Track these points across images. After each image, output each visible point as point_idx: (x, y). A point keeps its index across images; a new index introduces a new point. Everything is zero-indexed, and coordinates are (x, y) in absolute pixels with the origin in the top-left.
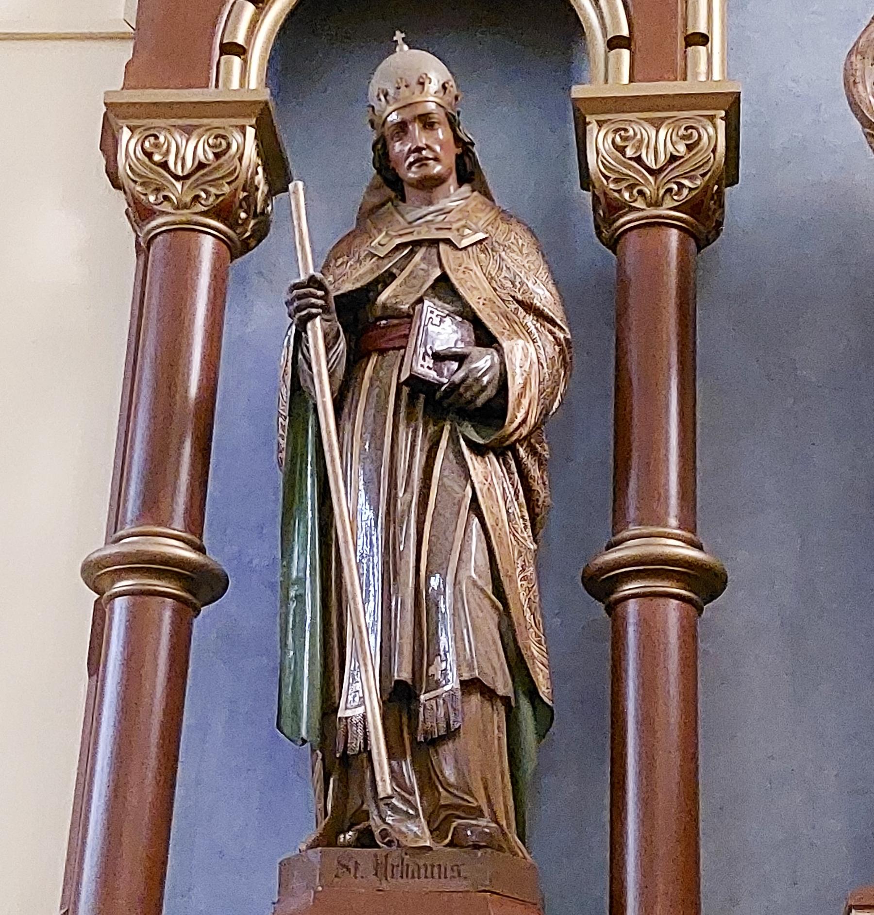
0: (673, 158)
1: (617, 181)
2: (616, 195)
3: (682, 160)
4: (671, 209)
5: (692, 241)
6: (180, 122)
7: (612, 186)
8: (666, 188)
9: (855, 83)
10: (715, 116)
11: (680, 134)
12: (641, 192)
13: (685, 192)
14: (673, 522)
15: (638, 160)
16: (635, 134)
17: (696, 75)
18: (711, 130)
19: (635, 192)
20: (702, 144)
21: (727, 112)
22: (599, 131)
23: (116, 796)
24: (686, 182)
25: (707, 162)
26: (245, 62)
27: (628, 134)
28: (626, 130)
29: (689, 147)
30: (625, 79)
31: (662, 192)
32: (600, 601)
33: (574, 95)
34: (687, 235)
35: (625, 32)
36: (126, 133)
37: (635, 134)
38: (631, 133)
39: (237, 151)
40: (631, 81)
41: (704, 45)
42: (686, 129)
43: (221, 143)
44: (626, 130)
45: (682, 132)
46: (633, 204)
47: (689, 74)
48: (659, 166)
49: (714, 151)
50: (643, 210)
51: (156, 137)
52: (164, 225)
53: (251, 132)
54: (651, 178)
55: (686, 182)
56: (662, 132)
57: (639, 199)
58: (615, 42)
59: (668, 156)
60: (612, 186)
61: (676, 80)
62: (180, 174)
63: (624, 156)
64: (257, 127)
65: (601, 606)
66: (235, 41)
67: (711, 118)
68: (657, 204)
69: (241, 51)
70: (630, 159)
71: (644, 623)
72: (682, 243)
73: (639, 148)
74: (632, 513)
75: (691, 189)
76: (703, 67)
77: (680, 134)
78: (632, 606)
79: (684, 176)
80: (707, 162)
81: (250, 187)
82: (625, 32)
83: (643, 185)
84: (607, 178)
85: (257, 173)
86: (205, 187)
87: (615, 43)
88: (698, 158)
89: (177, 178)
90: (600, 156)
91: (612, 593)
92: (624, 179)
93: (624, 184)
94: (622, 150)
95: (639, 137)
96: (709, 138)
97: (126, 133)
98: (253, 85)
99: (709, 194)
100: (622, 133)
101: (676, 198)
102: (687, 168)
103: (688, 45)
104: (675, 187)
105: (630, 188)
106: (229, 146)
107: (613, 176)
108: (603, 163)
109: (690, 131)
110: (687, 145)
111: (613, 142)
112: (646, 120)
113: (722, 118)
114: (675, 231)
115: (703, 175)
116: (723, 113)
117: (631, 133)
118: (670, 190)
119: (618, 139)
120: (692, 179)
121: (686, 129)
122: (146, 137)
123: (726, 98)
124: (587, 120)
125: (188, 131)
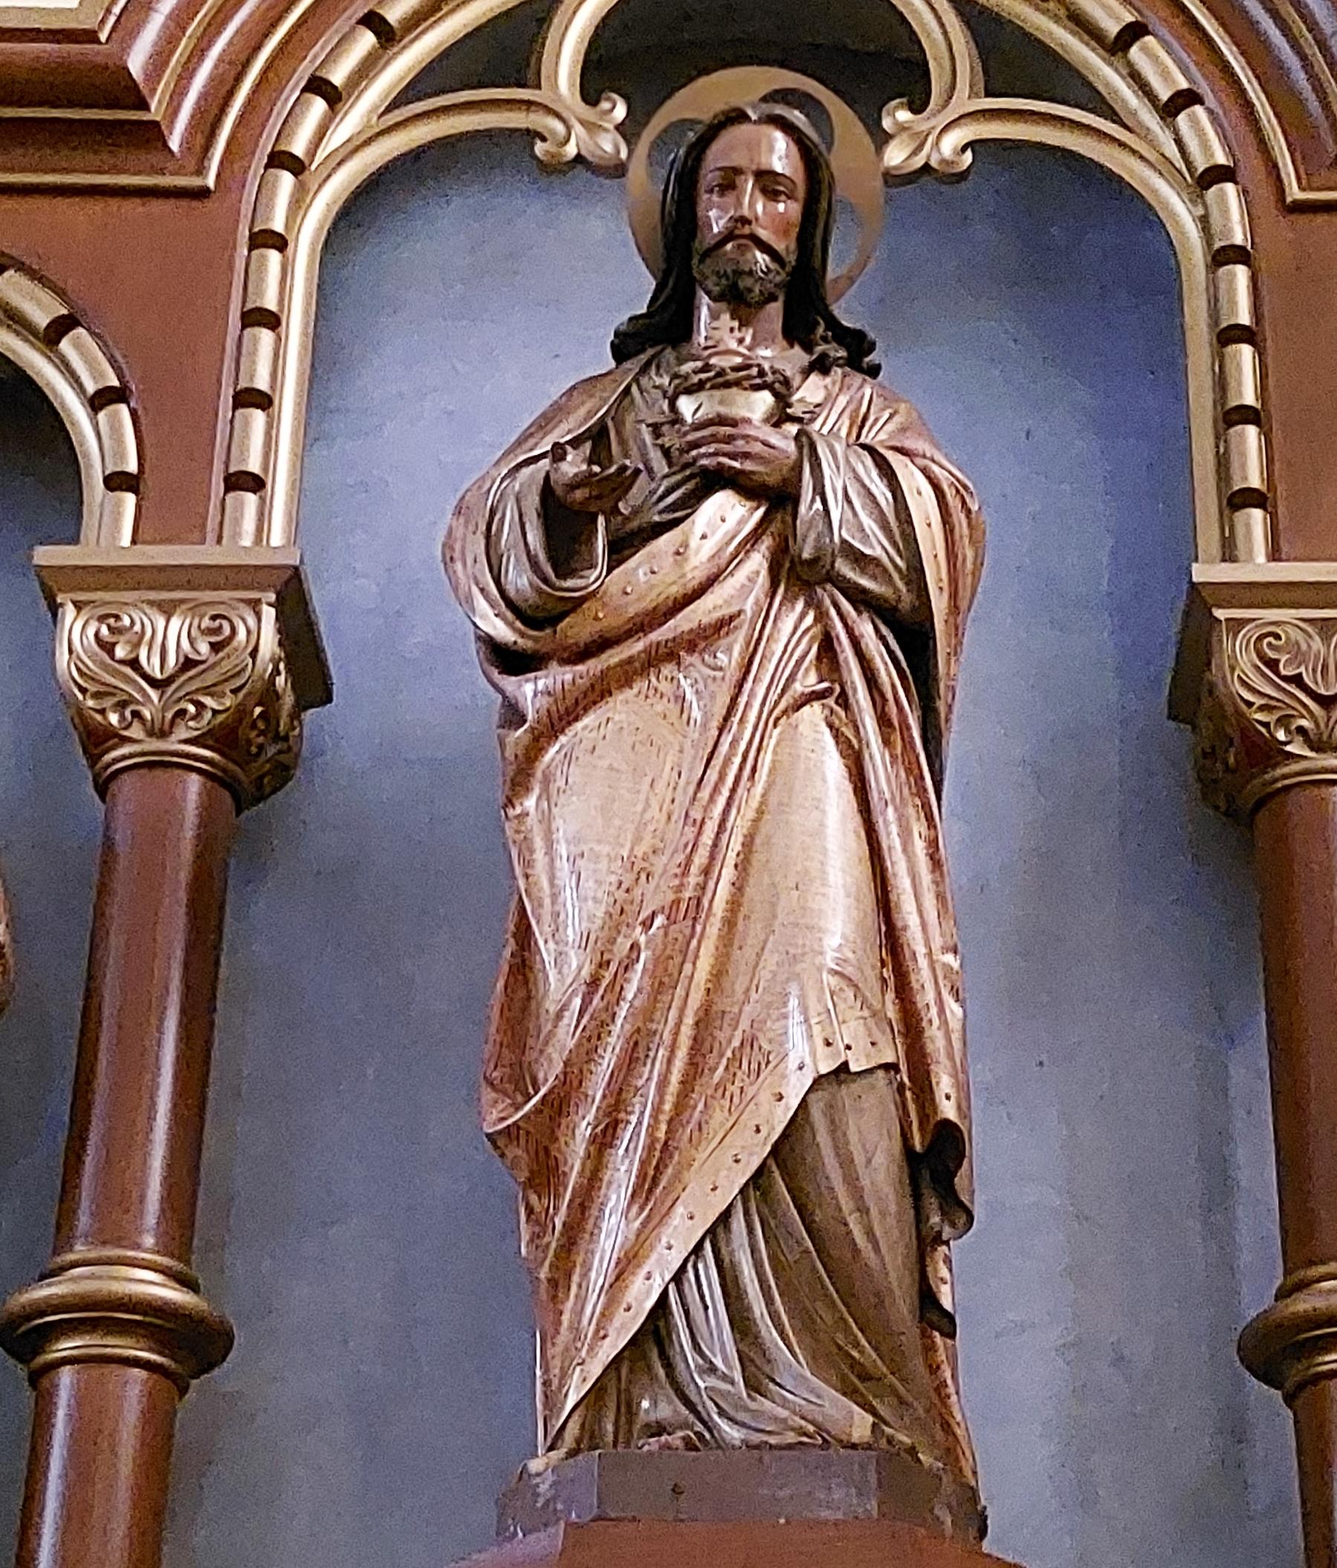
0: (188, 664)
1: (97, 695)
2: (99, 717)
3: (202, 667)
4: (186, 741)
5: (226, 796)
6: (153, 595)
7: (90, 703)
8: (177, 708)
9: (452, 559)
10: (259, 600)
11: (203, 626)
12: (136, 714)
13: (208, 715)
14: (149, 1241)
15: (134, 663)
16: (133, 623)
17: (237, 535)
18: (251, 621)
19: (128, 714)
20: (235, 644)
21: (278, 594)
22: (75, 619)
23: (151, 1098)
24: (208, 701)
25: (238, 673)
26: (262, 500)
27: (119, 624)
28: (1278, 637)
29: (215, 647)
30: (126, 540)
31: (169, 715)
32: (22, 1361)
33: (36, 561)
34: (216, 785)
35: (132, 467)
36: (70, 611)
37: (133, 623)
38: (127, 621)
39: (248, 641)
40: (134, 542)
41: (255, 492)
42: (214, 618)
43: (221, 626)
44: (1278, 637)
45: (206, 623)
46: (125, 733)
47: (226, 534)
48: (165, 675)
49: (254, 654)
50: (139, 743)
51: (117, 617)
52: (131, 756)
53: (269, 614)
54: (154, 694)
55: (208, 701)
56: (175, 622)
57: (136, 724)
58: (117, 481)
59: (182, 660)
60: (90, 703)
61: (203, 542)
62: (158, 675)
63: (113, 658)
64: (278, 605)
65: (22, 1372)
66: (243, 468)
67: (255, 605)
68: (163, 734)
69: (113, 484)
70: (122, 662)
71: (80, 1401)
72: (206, 795)
73: (137, 645)
74: (84, 1220)
75: (215, 712)
76: (249, 524)
77: (203, 626)
78: (66, 1377)
79: (207, 690)
80: (238, 673)
81: (268, 695)
82: (132, 467)
83: (138, 702)
84: (83, 691)
85: (279, 673)
86: (195, 697)
87: (117, 482)
88: (226, 666)
89: (153, 682)
90: (74, 656)
91: (39, 1354)
92: (1275, 707)
93: (108, 702)
94: (109, 648)
95: (137, 628)
96: (249, 632)
97: (70, 611)
98: (277, 538)
99: (247, 721)
100: (112, 621)
101: (191, 724)
102: (210, 678)
103: (228, 489)
104: (192, 709)
105: (121, 705)
106: (234, 631)
107: (92, 688)
108: (78, 669)
109: (217, 622)
110: (210, 643)
111: (97, 635)
112: (151, 603)
113: (270, 605)
114: (195, 777)
115: (235, 691)
116: (272, 597)
117: (127, 621)
118: (182, 713)
119: (104, 631)
120: (218, 696)
121: (214, 618)
122: (1260, 638)
123: (279, 572)
124: (59, 600)
125: (168, 610)
